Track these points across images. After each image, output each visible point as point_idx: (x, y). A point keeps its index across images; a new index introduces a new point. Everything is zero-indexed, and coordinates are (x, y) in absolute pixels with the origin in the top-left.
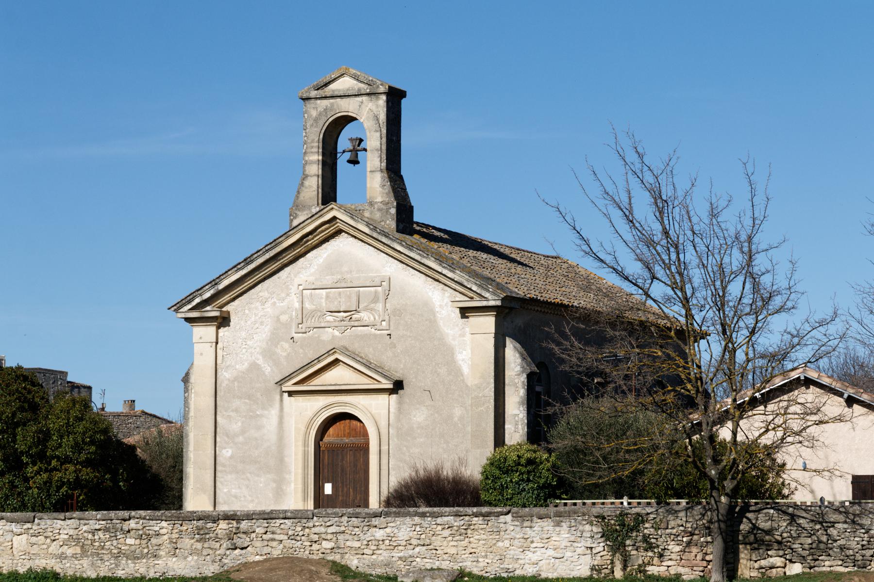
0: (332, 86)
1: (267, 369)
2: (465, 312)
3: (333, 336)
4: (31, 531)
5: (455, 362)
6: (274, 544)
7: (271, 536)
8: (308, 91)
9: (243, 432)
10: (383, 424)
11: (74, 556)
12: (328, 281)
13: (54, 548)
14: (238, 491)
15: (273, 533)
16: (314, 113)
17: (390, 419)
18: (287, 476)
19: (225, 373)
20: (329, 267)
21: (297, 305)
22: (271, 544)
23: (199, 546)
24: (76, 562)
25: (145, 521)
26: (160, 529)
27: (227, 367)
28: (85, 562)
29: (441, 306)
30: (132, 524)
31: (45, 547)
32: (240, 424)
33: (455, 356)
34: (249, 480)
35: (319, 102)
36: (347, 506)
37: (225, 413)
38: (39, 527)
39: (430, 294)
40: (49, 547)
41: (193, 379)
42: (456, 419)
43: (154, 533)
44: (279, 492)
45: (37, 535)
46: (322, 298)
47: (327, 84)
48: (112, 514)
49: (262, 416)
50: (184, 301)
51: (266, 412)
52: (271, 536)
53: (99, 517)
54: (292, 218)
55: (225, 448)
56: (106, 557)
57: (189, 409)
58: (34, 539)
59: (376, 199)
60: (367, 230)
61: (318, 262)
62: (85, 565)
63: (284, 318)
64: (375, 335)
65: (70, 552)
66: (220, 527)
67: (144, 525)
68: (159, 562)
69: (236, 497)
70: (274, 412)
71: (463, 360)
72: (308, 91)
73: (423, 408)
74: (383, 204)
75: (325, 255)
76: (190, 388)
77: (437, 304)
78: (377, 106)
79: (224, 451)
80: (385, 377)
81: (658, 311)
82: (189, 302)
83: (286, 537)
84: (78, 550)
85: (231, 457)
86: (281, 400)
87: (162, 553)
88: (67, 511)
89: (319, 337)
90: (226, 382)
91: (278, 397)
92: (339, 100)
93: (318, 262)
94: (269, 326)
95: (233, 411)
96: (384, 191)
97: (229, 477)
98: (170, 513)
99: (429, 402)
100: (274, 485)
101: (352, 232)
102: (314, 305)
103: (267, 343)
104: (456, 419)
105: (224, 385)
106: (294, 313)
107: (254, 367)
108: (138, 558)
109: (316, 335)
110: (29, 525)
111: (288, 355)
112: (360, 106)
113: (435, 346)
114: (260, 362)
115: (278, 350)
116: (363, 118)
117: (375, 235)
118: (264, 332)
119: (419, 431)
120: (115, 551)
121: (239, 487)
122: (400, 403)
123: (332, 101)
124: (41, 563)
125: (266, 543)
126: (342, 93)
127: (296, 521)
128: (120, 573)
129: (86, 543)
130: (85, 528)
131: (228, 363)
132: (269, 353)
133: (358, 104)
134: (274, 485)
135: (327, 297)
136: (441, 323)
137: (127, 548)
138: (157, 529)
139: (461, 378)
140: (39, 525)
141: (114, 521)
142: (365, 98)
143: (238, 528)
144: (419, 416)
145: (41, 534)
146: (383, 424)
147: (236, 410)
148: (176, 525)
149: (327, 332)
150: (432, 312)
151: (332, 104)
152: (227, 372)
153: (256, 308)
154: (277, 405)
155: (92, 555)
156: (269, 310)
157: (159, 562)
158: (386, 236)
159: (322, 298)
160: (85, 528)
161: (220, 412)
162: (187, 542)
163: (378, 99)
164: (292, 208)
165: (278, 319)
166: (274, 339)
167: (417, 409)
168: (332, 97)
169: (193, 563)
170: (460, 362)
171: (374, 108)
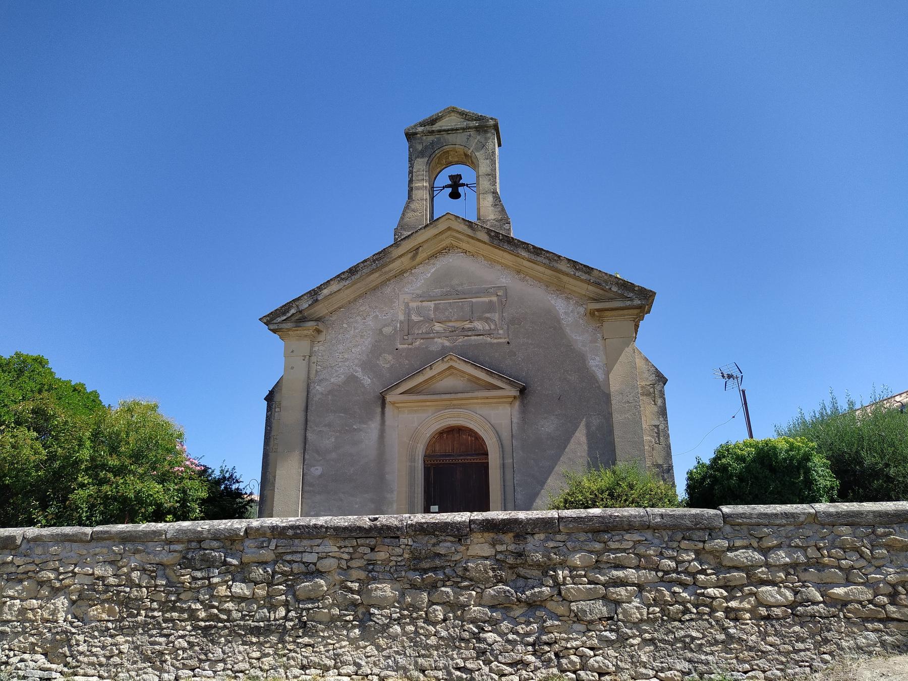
1: (367, 381)
3: (443, 346)
5: (588, 369)
10: (506, 435)
17: (514, 430)
18: (389, 496)
19: (318, 387)
21: (401, 317)
25: (282, 542)
26: (319, 558)
27: (320, 381)
29: (565, 313)
33: (587, 362)
34: (341, 500)
37: (316, 428)
38: (28, 560)
39: (553, 302)
41: (277, 398)
43: (303, 568)
45: (20, 576)
46: (429, 310)
49: (360, 430)
54: (397, 237)
55: (314, 466)
57: (271, 428)
59: (489, 216)
61: (425, 277)
63: (387, 330)
67: (280, 550)
70: (374, 426)
71: (597, 366)
73: (553, 418)
74: (497, 221)
76: (273, 407)
77: (561, 311)
79: (313, 469)
80: (511, 383)
82: (284, 313)
89: (426, 348)
90: (319, 396)
93: (425, 277)
94: (369, 339)
95: (325, 426)
96: (496, 210)
102: (421, 317)
103: (368, 355)
105: (316, 399)
106: (398, 325)
107: (352, 379)
109: (424, 346)
111: (392, 366)
112: (468, 139)
113: (562, 353)
114: (359, 374)
115: (381, 362)
116: (472, 149)
118: (367, 342)
119: (549, 442)
121: (330, 509)
131: (321, 377)
132: (369, 365)
133: (466, 137)
135: (436, 308)
136: (568, 330)
138: (310, 558)
139: (597, 385)
143: (520, 555)
145: (30, 574)
146: (506, 435)
147: (329, 425)
148: (361, 550)
149: (436, 342)
150: (558, 321)
151: (439, 139)
152: (320, 386)
153: (356, 322)
156: (370, 323)
159: (429, 310)
161: (311, 427)
164: (397, 229)
165: (381, 331)
166: (376, 350)
167: (546, 418)
170: (594, 368)
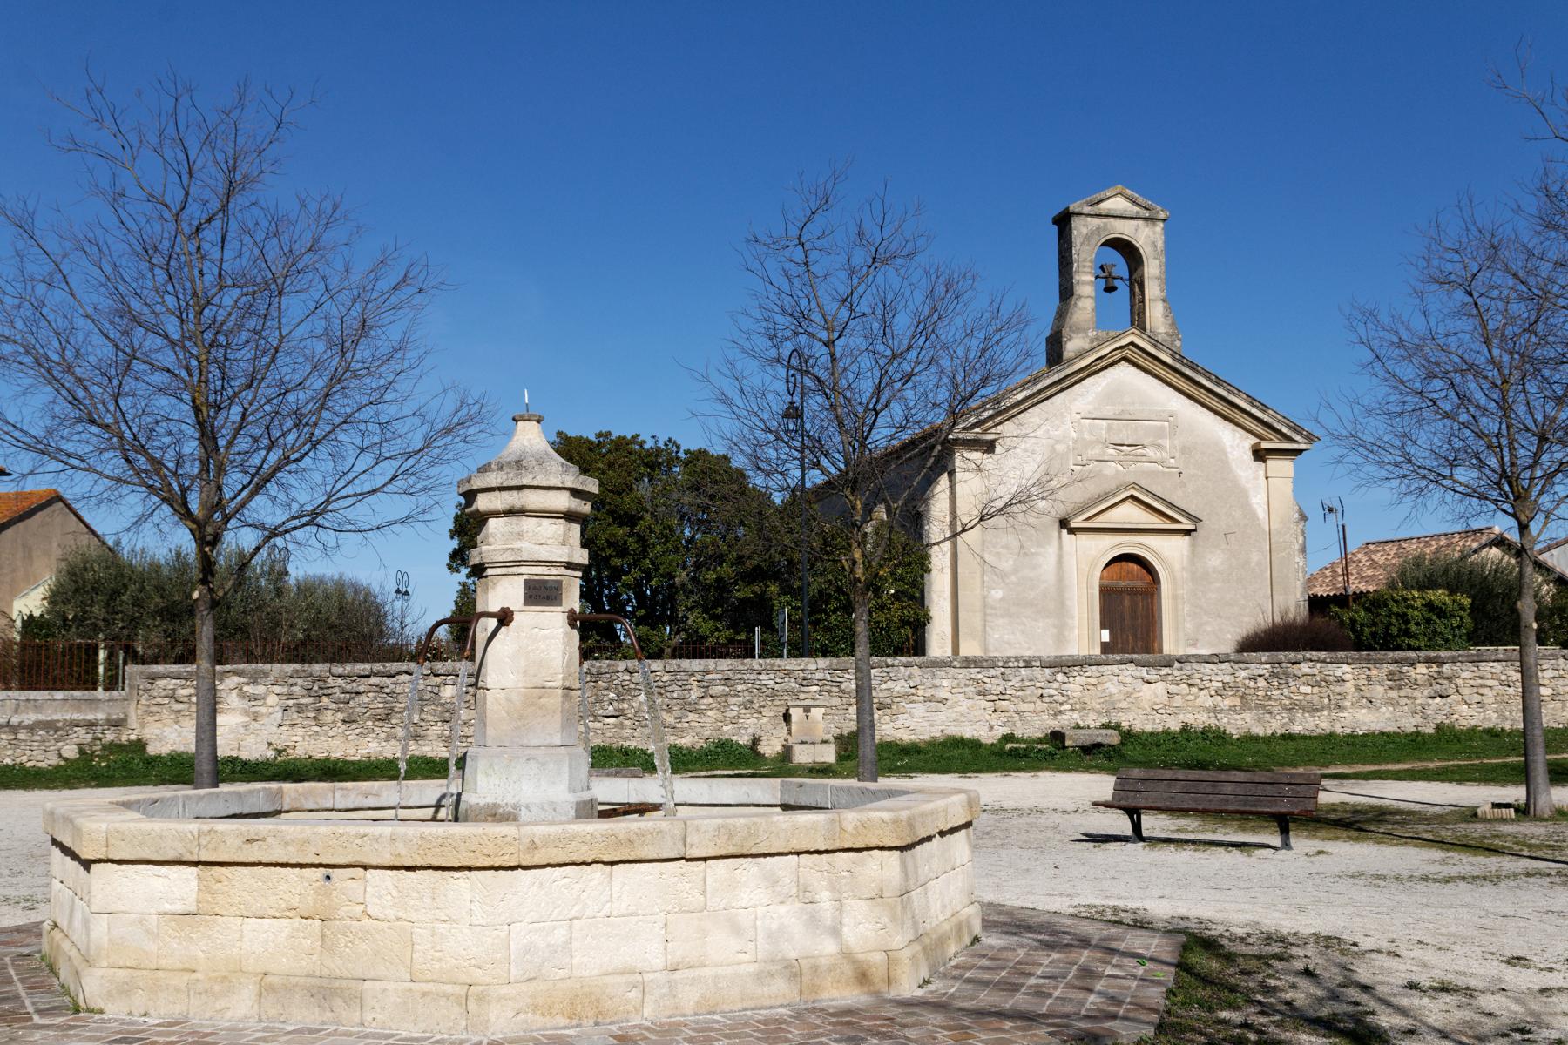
0: (1104, 205)
2: (1259, 455)
4: (1170, 678)
6: (1485, 691)
7: (1480, 681)
8: (1081, 206)
9: (1016, 571)
11: (1232, 709)
12: (1108, 411)
13: (1205, 699)
14: (1012, 637)
15: (1482, 678)
16: (1085, 231)
18: (1070, 621)
20: (1111, 396)
22: (1481, 691)
23: (1393, 694)
24: (1237, 717)
28: (1248, 716)
29: (1232, 447)
30: (1305, 668)
31: (1192, 697)
32: (1011, 562)
35: (1089, 219)
36: (1124, 652)
40: (1197, 697)
42: (1253, 564)
44: (1060, 638)
47: (1098, 203)
48: (1281, 656)
50: (990, 424)
51: (1042, 550)
52: (1480, 681)
53: (1264, 659)
56: (1275, 710)
58: (1173, 689)
60: (1168, 360)
62: (1248, 720)
64: (1163, 473)
65: (1227, 703)
66: (1418, 671)
68: (1345, 714)
69: (1009, 644)
70: (1051, 551)
72: (1081, 206)
75: (1104, 384)
78: (1155, 233)
81: (435, 444)
83: (1497, 683)
84: (1237, 702)
85: (1002, 599)
86: (1060, 537)
87: (1348, 704)
88: (347, 661)
91: (1055, 534)
92: (1112, 220)
97: (1001, 621)
98: (743, 664)
99: (1224, 546)
100: (1055, 631)
101: (1141, 361)
104: (1253, 564)
108: (1318, 710)
110: (1165, 671)
117: (1178, 366)
120: (1287, 702)
122: (1193, 545)
123: (1104, 220)
124: (1199, 720)
125: (1475, 690)
126: (1118, 214)
127: (1056, 670)
128: (1296, 729)
129: (1247, 692)
130: (1244, 674)
134: (1054, 631)
136: (1233, 465)
137: (1301, 697)
138: (1338, 674)
140: (1181, 669)
141: (1284, 665)
142: (1140, 222)
143: (1439, 673)
144: (1214, 560)
147: (1006, 547)
151: (1105, 224)
154: (1055, 542)
155: (1257, 708)
157: (1345, 714)
158: (1192, 368)
160: (1244, 674)
162: (1378, 691)
163: (1155, 225)
168: (1107, 216)
169: (1387, 715)
171: (1151, 233)
